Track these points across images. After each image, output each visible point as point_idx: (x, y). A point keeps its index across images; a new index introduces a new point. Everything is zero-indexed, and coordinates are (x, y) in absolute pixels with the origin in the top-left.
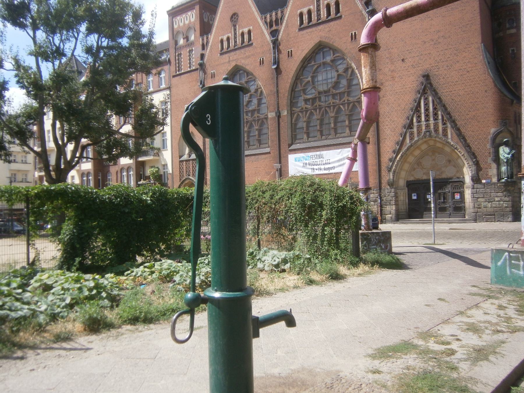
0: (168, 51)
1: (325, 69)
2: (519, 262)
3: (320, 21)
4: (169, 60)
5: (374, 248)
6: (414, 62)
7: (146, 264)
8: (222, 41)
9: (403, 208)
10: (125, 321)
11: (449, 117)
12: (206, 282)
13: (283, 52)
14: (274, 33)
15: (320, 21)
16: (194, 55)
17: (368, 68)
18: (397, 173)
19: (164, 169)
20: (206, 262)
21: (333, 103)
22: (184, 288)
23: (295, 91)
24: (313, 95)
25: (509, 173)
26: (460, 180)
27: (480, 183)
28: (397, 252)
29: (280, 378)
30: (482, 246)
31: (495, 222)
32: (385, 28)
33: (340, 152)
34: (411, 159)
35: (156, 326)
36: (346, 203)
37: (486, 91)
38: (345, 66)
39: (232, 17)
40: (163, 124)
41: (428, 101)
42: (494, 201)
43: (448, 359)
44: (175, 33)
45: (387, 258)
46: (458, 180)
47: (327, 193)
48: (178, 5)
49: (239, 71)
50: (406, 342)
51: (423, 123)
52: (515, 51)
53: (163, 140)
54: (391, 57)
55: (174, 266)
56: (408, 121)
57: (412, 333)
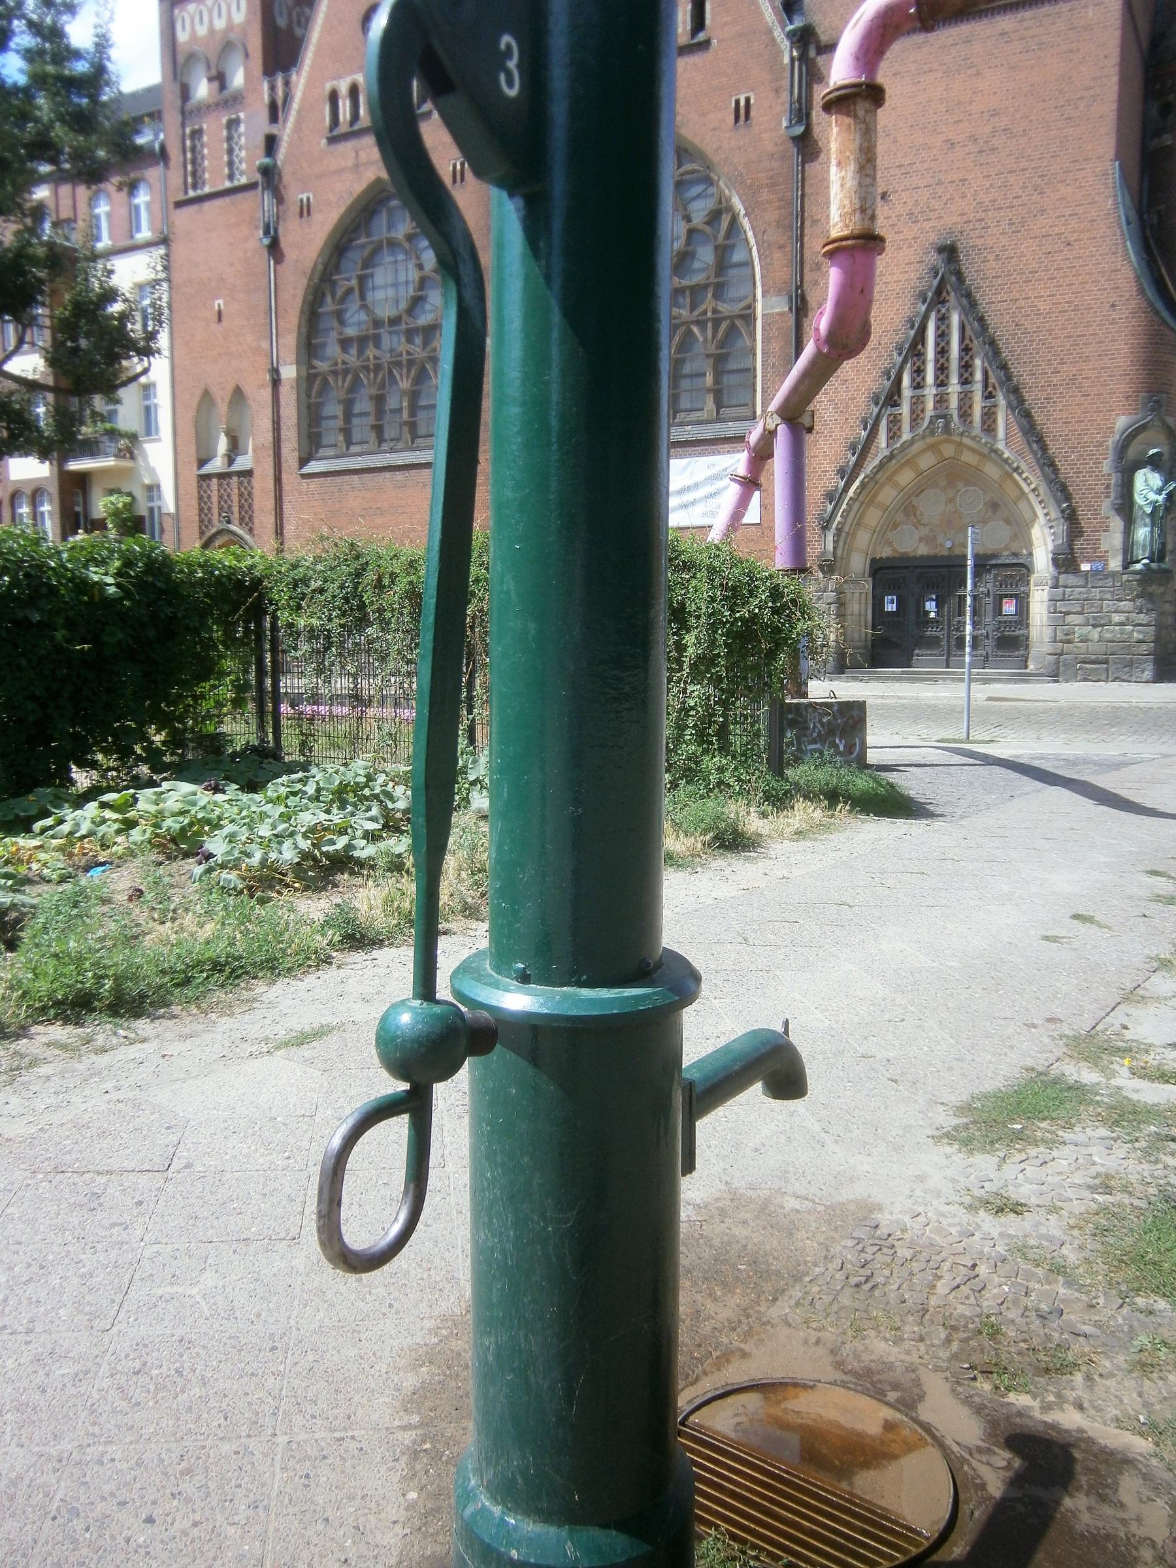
4: (163, 148)
5: (815, 750)
7: (109, 797)
8: (334, 97)
10: (44, 1010)
12: (314, 859)
17: (852, 167)
18: (848, 534)
19: (151, 499)
20: (310, 789)
25: (1156, 547)
26: (1021, 561)
31: (1106, 681)
33: (685, 468)
36: (760, 608)
37: (1113, 306)
40: (147, 352)
42: (1110, 623)
44: (181, 59)
45: (862, 783)
47: (698, 575)
50: (1040, 1074)
51: (930, 391)
53: (148, 409)
55: (202, 803)
56: (887, 384)
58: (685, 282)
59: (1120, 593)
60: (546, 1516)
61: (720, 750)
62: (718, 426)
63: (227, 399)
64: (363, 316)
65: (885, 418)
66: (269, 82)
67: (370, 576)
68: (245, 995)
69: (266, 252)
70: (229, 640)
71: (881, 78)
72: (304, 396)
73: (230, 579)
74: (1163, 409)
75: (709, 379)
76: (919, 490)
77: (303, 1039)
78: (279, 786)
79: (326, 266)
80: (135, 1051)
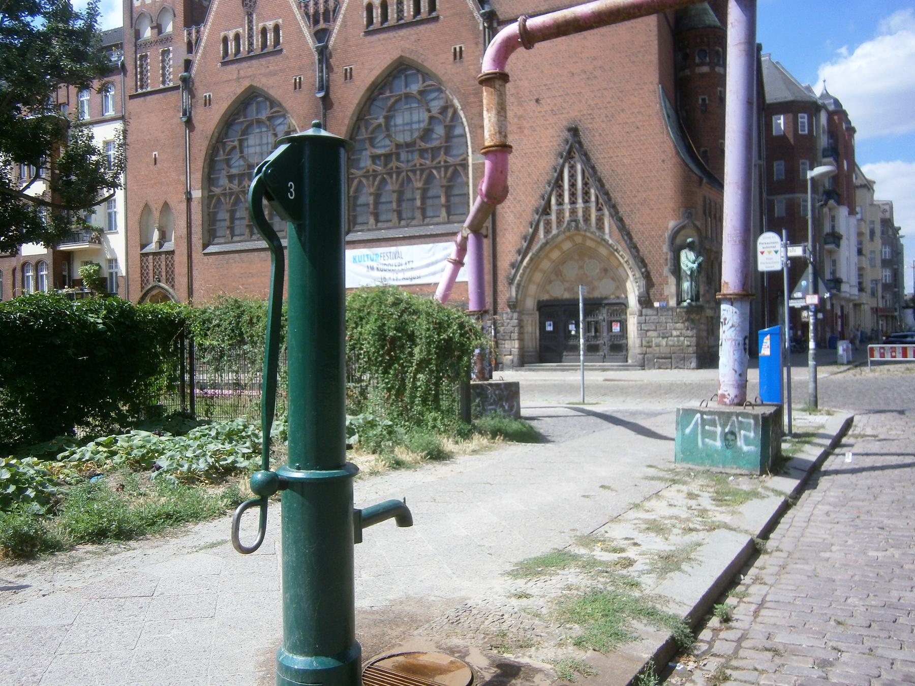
0: (122, 48)
3: (402, 22)
4: (123, 65)
5: (492, 409)
6: (555, 105)
8: (225, 40)
9: (530, 345)
10: (82, 538)
11: (608, 200)
12: (216, 468)
13: (336, 69)
14: (321, 35)
15: (402, 22)
16: (171, 61)
17: (494, 112)
18: (524, 286)
19: (111, 267)
20: (213, 433)
21: (421, 165)
24: (387, 149)
26: (621, 301)
27: (652, 306)
28: (527, 415)
29: (373, 613)
30: (654, 405)
31: (671, 368)
34: (546, 265)
35: (142, 543)
36: (453, 334)
38: (441, 103)
41: (576, 171)
42: (671, 336)
43: (624, 572)
44: (135, 16)
45: (515, 426)
46: (618, 301)
49: (256, 97)
50: (559, 551)
51: (567, 207)
52: (707, 102)
53: (110, 214)
54: (518, 94)
56: (543, 203)
57: (567, 538)
58: (428, 146)
59: (676, 319)
60: (306, 654)
61: (436, 408)
62: (448, 226)
63: (159, 209)
64: (242, 163)
67: (246, 317)
70: (166, 353)
71: (507, 69)
72: (206, 208)
75: (443, 200)
76: (564, 261)
77: (213, 545)
78: (196, 432)
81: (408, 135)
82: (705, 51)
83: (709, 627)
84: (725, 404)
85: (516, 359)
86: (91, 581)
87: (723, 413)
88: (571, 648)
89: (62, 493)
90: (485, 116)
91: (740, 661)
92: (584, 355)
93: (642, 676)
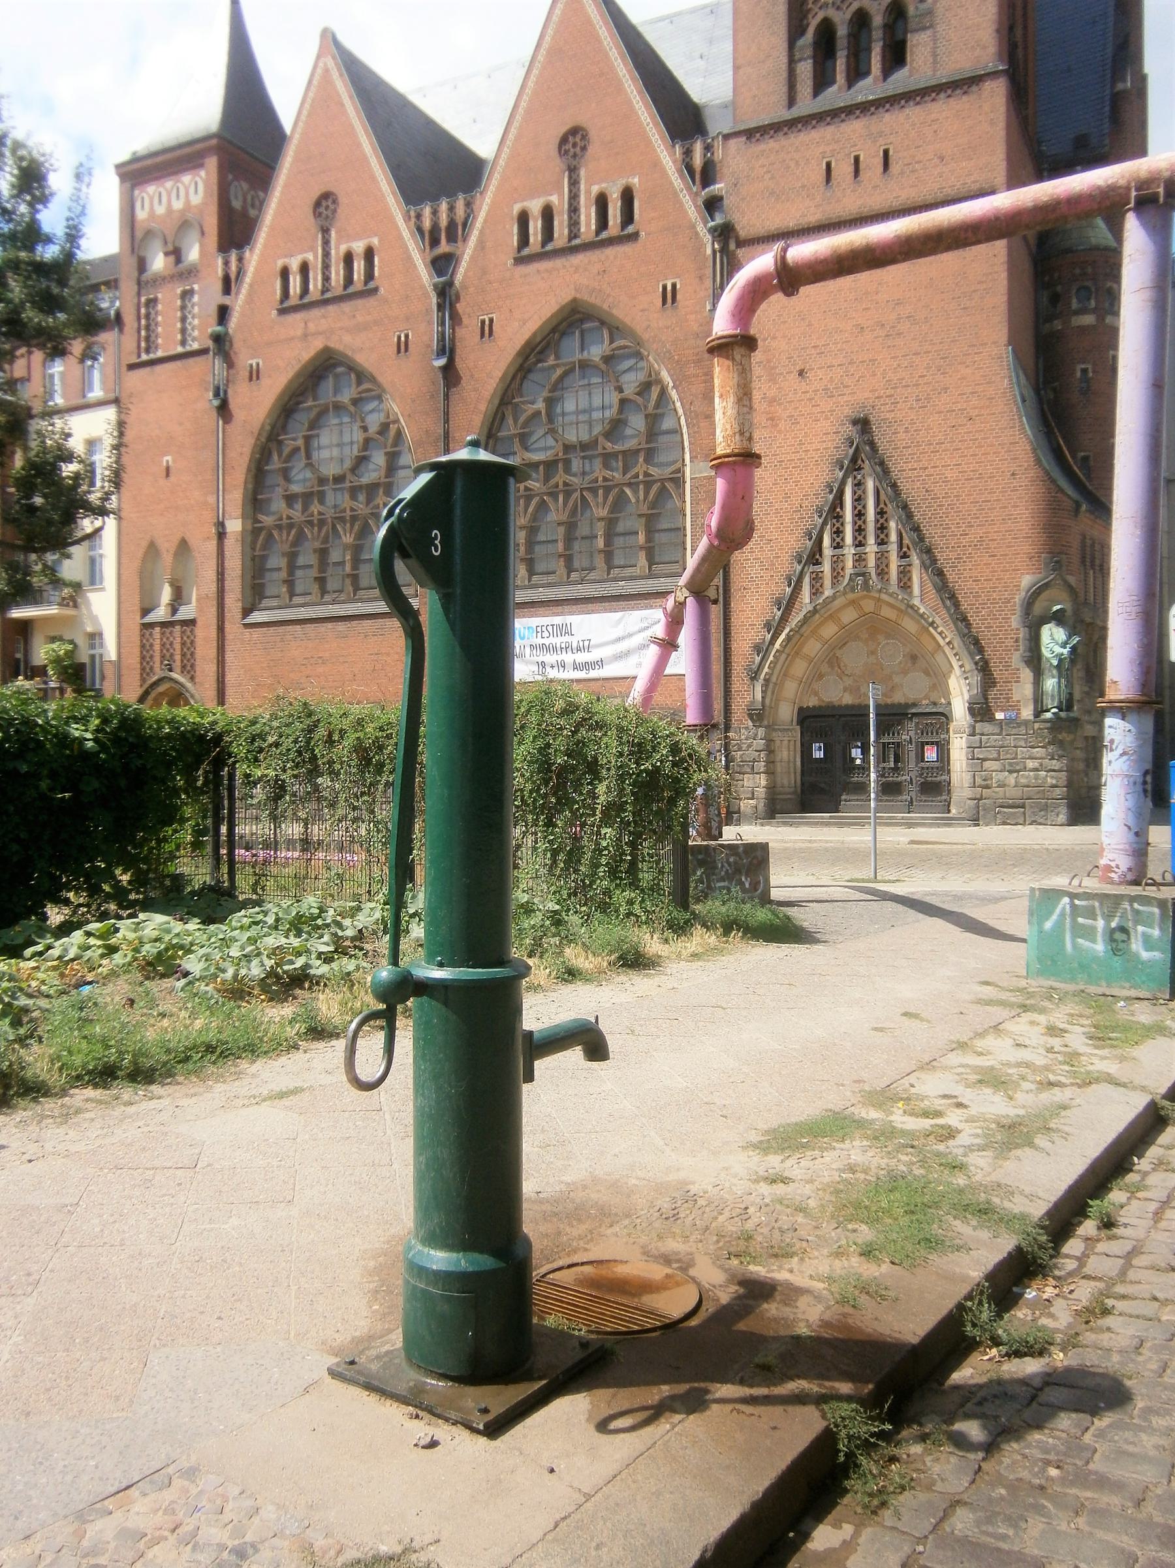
0: (116, 287)
1: (586, 382)
2: (1095, 919)
3: (577, 242)
4: (118, 315)
5: (724, 888)
6: (831, 380)
8: (285, 273)
9: (786, 782)
10: (79, 1077)
12: (277, 976)
13: (465, 320)
14: (442, 264)
15: (577, 242)
17: (732, 399)
18: (775, 684)
19: (92, 647)
20: (270, 920)
21: (605, 479)
22: (219, 991)
23: (497, 439)
24: (549, 453)
26: (941, 710)
27: (991, 719)
28: (781, 899)
29: (541, 1202)
30: (997, 886)
31: (1024, 824)
32: (779, 296)
33: (620, 620)
34: (813, 647)
36: (662, 762)
37: (1013, 474)
38: (641, 376)
39: (318, 204)
42: (1025, 769)
43: (941, 1147)
44: (139, 234)
45: (762, 915)
46: (934, 710)
47: (609, 733)
48: (153, 149)
49: (335, 366)
51: (849, 551)
52: (1091, 375)
56: (809, 544)
57: (848, 1094)
62: (650, 581)
64: (309, 474)
65: (808, 575)
66: (223, 258)
67: (322, 732)
68: (233, 1069)
69: (215, 414)
72: (248, 549)
73: (194, 734)
74: (1064, 568)
75: (641, 538)
76: (847, 637)
77: (282, 1095)
78: (240, 917)
79: (273, 427)
80: (153, 1104)
81: (583, 428)
82: (1087, 288)
83: (1080, 1236)
84: (1112, 882)
85: (761, 806)
86: (99, 1142)
87: (1107, 896)
88: (855, 1260)
89: (40, 1008)
90: (717, 407)
91: (1128, 1286)
92: (876, 800)
93: (969, 1304)
